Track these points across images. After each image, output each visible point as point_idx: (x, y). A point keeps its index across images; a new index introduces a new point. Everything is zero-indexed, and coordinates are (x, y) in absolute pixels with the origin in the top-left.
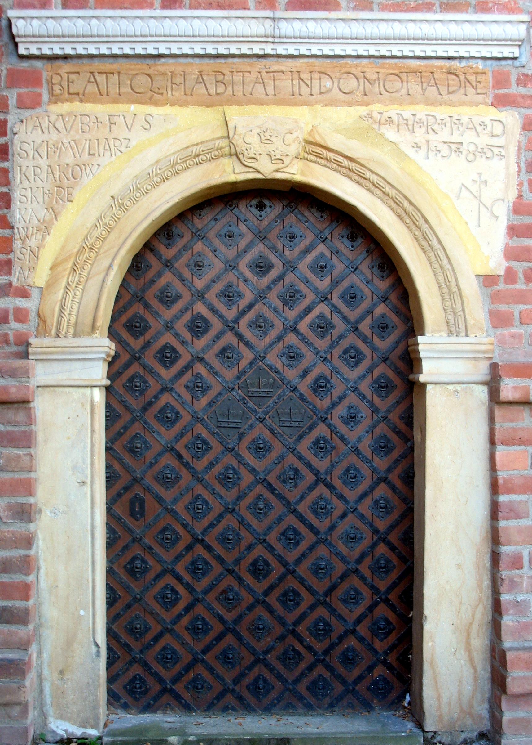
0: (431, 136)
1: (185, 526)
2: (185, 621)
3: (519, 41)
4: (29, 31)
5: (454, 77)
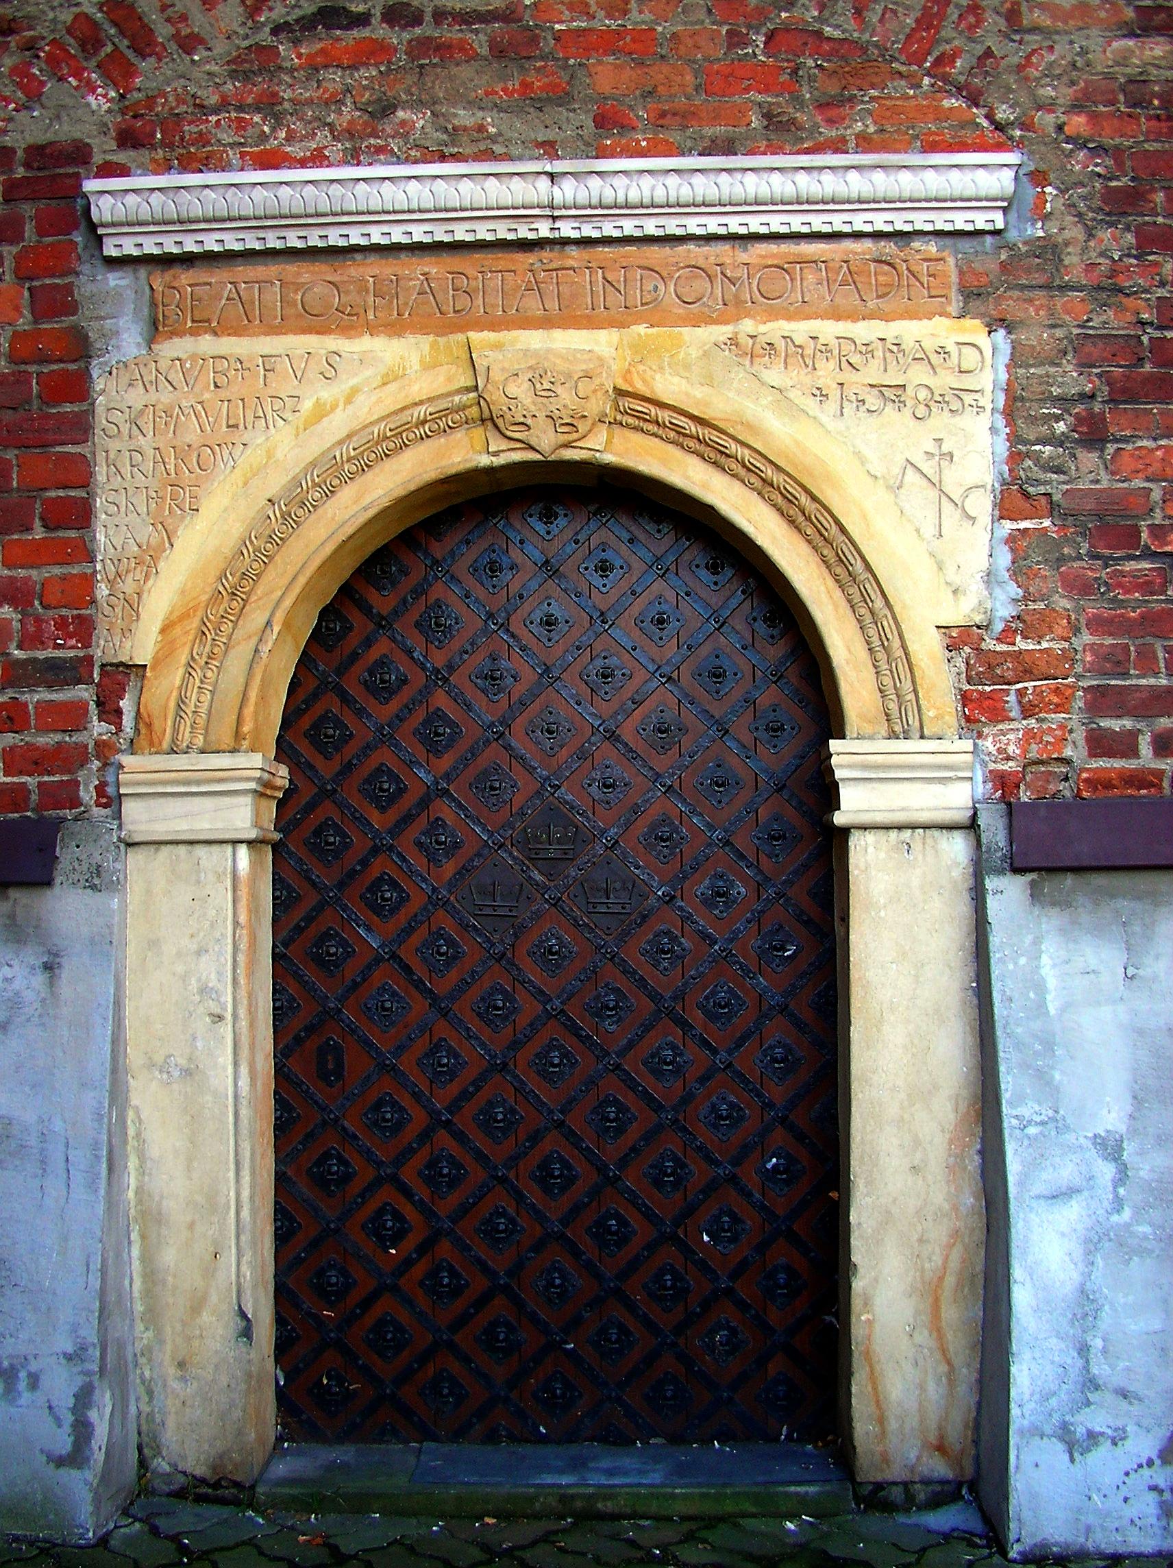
0: (848, 376)
1: (417, 1096)
2: (419, 1270)
3: (1003, 200)
4: (120, 214)
5: (886, 268)
